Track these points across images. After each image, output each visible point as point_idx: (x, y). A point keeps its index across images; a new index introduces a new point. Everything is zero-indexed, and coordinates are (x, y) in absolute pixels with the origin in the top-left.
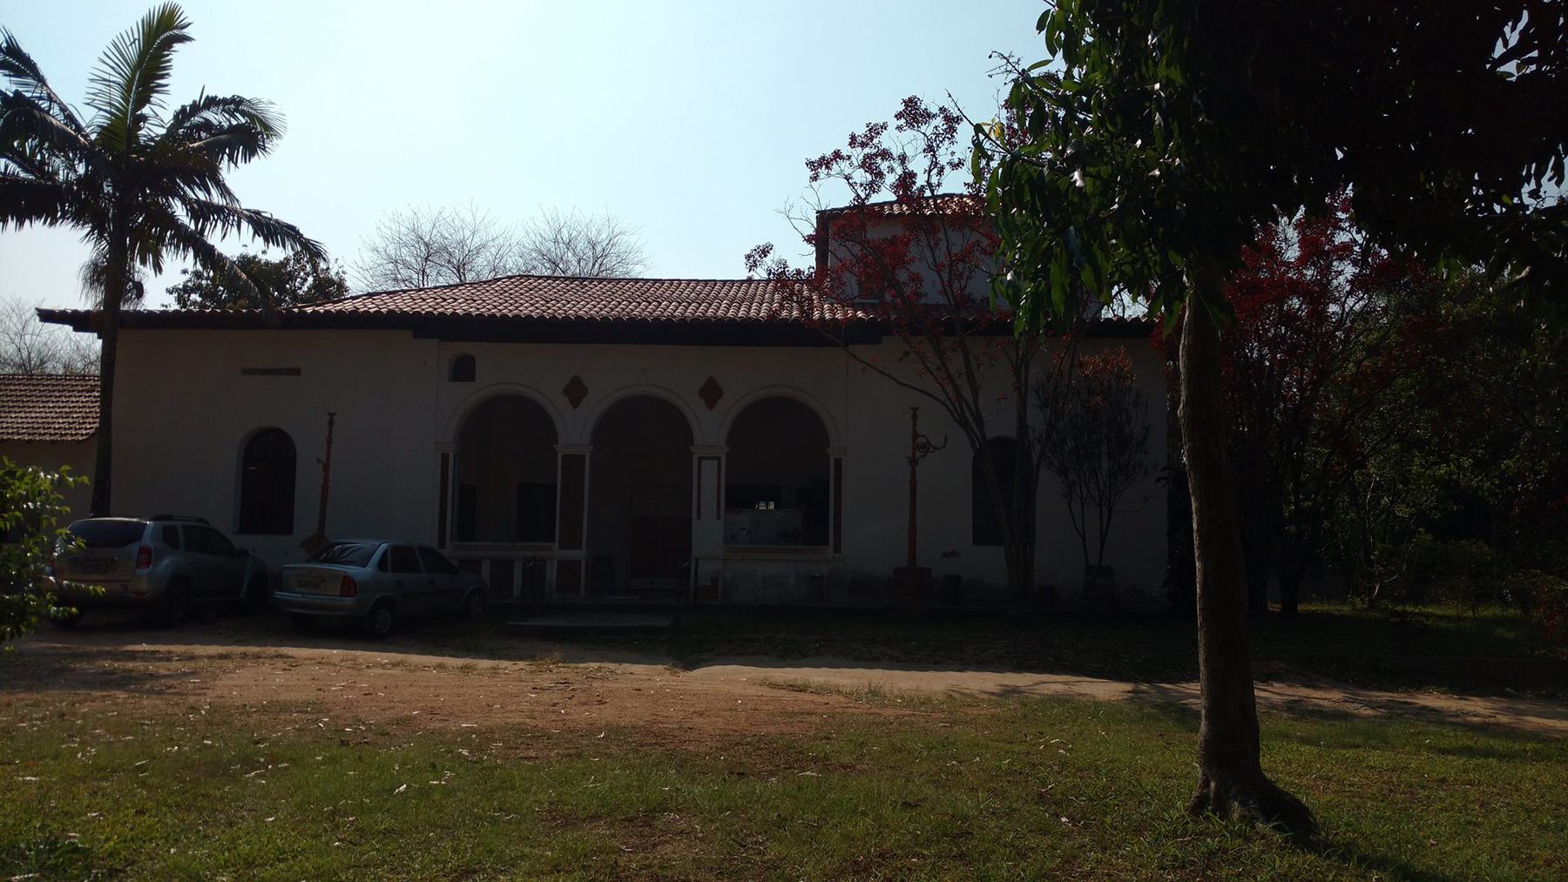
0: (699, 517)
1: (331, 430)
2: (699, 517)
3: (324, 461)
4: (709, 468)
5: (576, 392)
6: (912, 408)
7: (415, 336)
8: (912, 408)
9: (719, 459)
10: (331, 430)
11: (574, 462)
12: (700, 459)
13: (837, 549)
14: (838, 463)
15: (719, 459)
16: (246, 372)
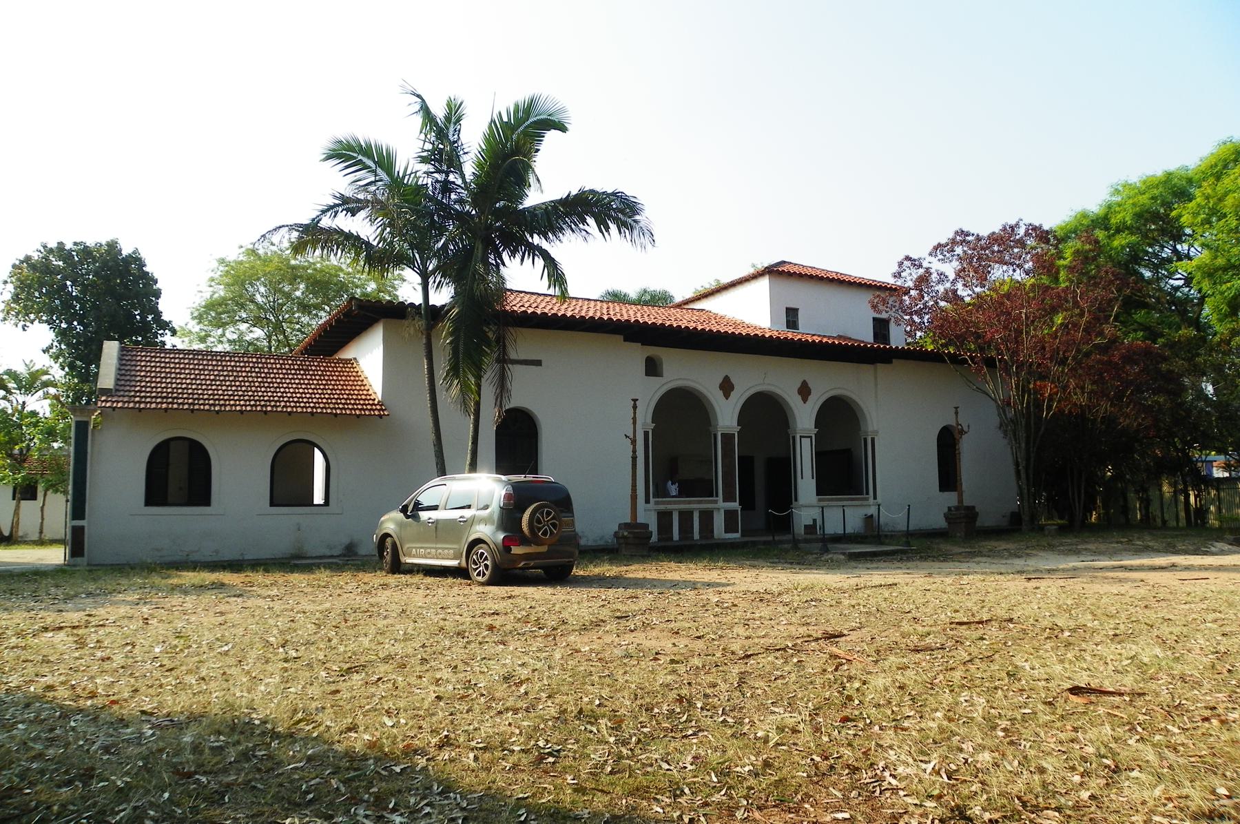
1: (635, 413)
3: (632, 437)
4: (806, 442)
5: (727, 387)
6: (633, 400)
7: (625, 340)
8: (633, 400)
9: (811, 437)
10: (635, 413)
11: (727, 438)
12: (801, 437)
13: (875, 498)
14: (873, 440)
15: (811, 437)
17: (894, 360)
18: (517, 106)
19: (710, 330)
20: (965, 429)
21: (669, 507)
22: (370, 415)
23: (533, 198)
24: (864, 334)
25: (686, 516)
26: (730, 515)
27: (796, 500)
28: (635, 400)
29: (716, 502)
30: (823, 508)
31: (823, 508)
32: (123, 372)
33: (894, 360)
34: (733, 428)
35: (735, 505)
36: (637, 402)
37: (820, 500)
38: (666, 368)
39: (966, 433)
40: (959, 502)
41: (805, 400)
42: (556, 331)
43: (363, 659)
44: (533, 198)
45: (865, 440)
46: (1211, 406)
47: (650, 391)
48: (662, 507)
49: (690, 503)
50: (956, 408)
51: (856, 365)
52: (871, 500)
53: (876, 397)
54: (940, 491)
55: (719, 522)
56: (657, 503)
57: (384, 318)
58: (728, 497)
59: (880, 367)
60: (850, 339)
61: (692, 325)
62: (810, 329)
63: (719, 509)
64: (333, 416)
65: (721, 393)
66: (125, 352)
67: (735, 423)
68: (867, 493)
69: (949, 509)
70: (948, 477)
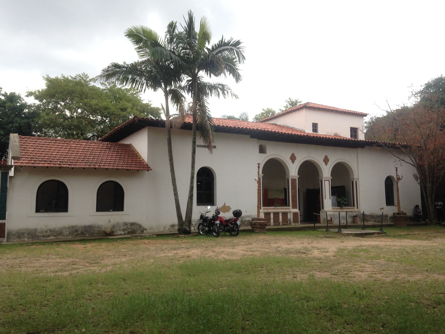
0: (325, 199)
2: (325, 199)
4: (327, 183)
9: (329, 181)
11: (293, 180)
12: (325, 180)
13: (357, 208)
14: (356, 182)
17: (365, 146)
18: (211, 38)
19: (278, 132)
20: (401, 178)
21: (270, 211)
22: (122, 169)
23: (212, 74)
24: (346, 135)
25: (276, 215)
26: (295, 214)
27: (323, 208)
28: (397, 168)
29: (289, 209)
30: (339, 213)
31: (339, 213)
32: (23, 149)
33: (365, 146)
34: (329, 178)
35: (297, 210)
36: (260, 165)
37: (333, 209)
38: (268, 151)
39: (401, 179)
40: (398, 211)
41: (326, 164)
42: (188, 130)
43: (234, 253)
44: (212, 74)
45: (353, 182)
46: (72, 129)
47: (263, 159)
48: (266, 211)
49: (269, 209)
50: (259, 164)
51: (296, 144)
52: (356, 209)
53: (358, 164)
54: (387, 205)
55: (290, 216)
56: (264, 209)
57: (148, 126)
58: (294, 207)
59: (359, 149)
60: (341, 137)
61: (270, 130)
62: (322, 132)
63: (290, 212)
64: (94, 169)
65: (324, 163)
66: (21, 139)
67: (330, 176)
68: (354, 206)
69: (394, 214)
70: (390, 201)
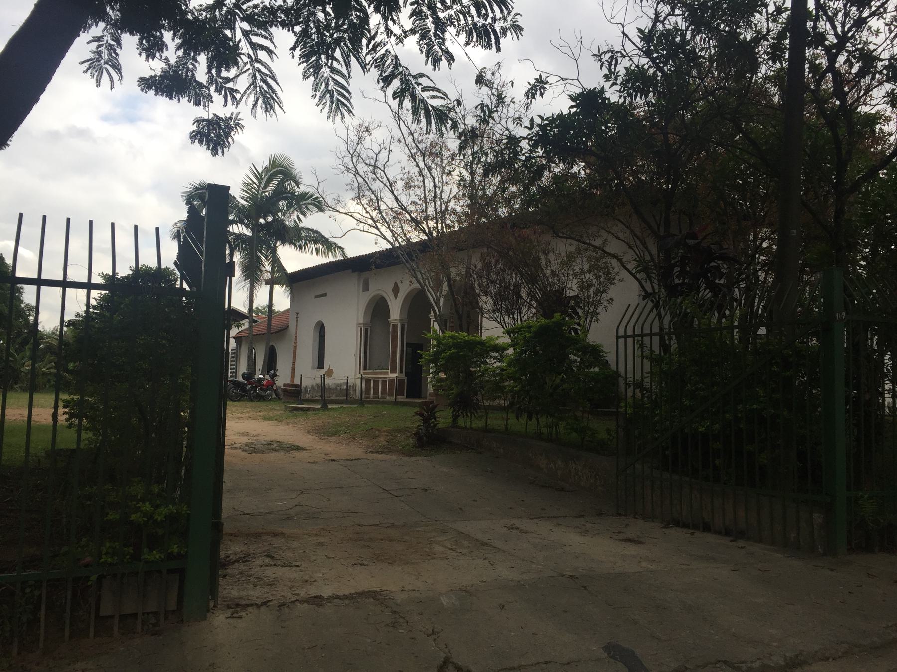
16: (317, 296)
29: (387, 373)
58: (393, 371)
